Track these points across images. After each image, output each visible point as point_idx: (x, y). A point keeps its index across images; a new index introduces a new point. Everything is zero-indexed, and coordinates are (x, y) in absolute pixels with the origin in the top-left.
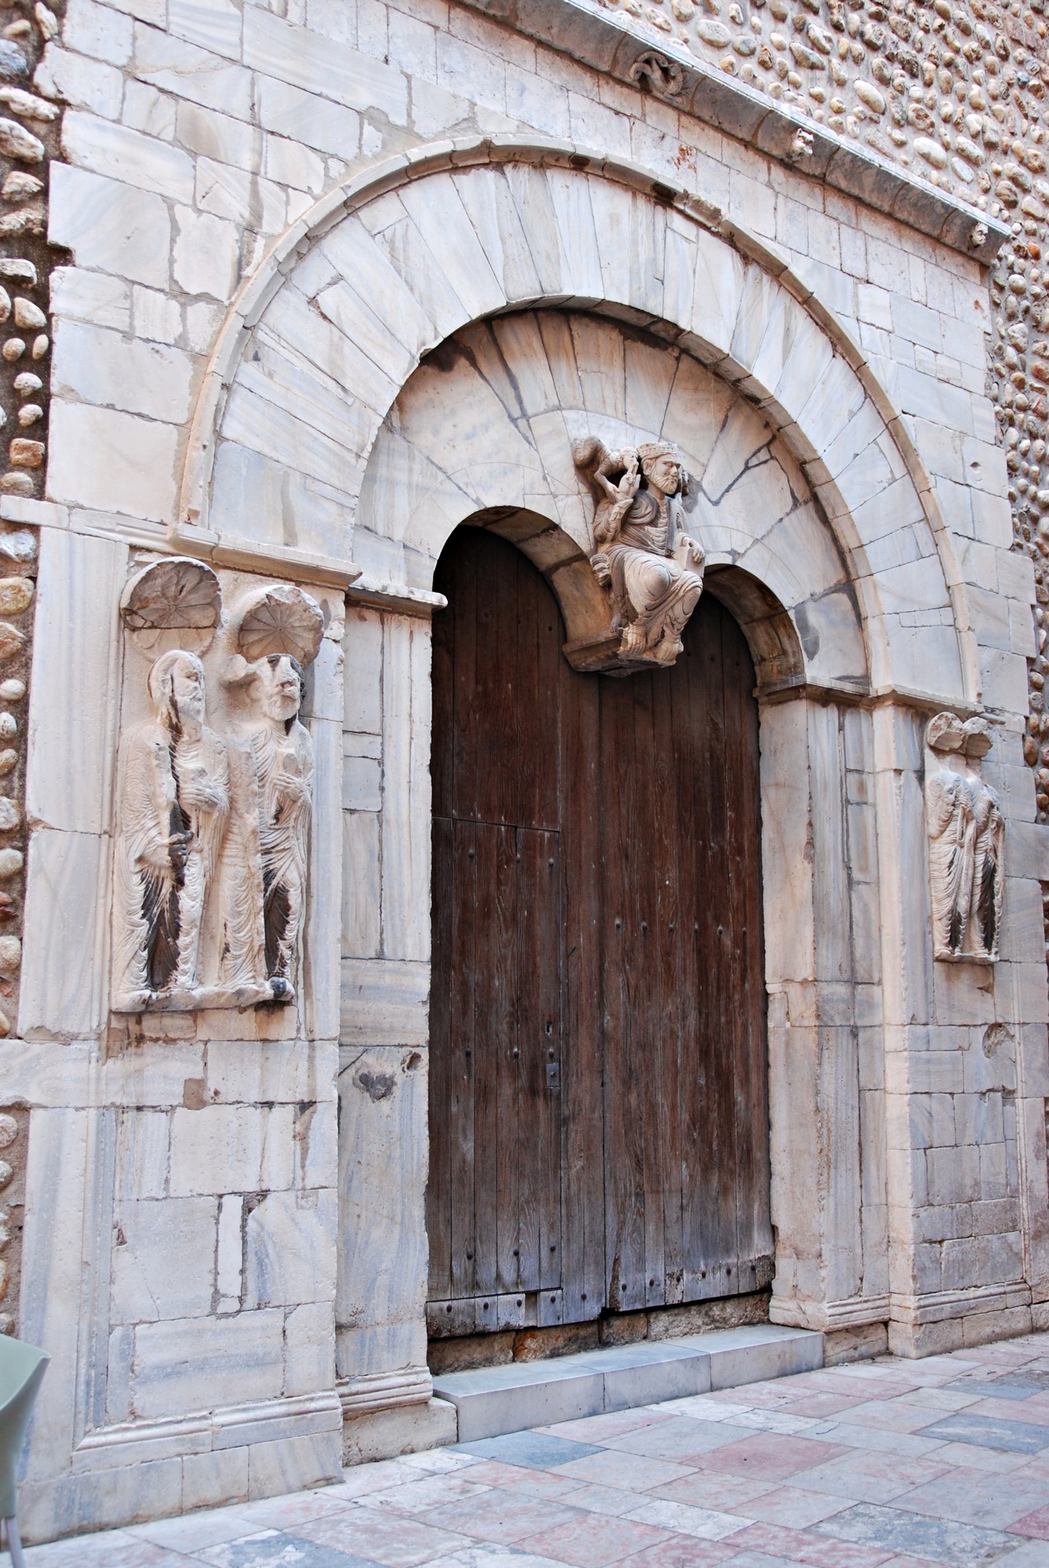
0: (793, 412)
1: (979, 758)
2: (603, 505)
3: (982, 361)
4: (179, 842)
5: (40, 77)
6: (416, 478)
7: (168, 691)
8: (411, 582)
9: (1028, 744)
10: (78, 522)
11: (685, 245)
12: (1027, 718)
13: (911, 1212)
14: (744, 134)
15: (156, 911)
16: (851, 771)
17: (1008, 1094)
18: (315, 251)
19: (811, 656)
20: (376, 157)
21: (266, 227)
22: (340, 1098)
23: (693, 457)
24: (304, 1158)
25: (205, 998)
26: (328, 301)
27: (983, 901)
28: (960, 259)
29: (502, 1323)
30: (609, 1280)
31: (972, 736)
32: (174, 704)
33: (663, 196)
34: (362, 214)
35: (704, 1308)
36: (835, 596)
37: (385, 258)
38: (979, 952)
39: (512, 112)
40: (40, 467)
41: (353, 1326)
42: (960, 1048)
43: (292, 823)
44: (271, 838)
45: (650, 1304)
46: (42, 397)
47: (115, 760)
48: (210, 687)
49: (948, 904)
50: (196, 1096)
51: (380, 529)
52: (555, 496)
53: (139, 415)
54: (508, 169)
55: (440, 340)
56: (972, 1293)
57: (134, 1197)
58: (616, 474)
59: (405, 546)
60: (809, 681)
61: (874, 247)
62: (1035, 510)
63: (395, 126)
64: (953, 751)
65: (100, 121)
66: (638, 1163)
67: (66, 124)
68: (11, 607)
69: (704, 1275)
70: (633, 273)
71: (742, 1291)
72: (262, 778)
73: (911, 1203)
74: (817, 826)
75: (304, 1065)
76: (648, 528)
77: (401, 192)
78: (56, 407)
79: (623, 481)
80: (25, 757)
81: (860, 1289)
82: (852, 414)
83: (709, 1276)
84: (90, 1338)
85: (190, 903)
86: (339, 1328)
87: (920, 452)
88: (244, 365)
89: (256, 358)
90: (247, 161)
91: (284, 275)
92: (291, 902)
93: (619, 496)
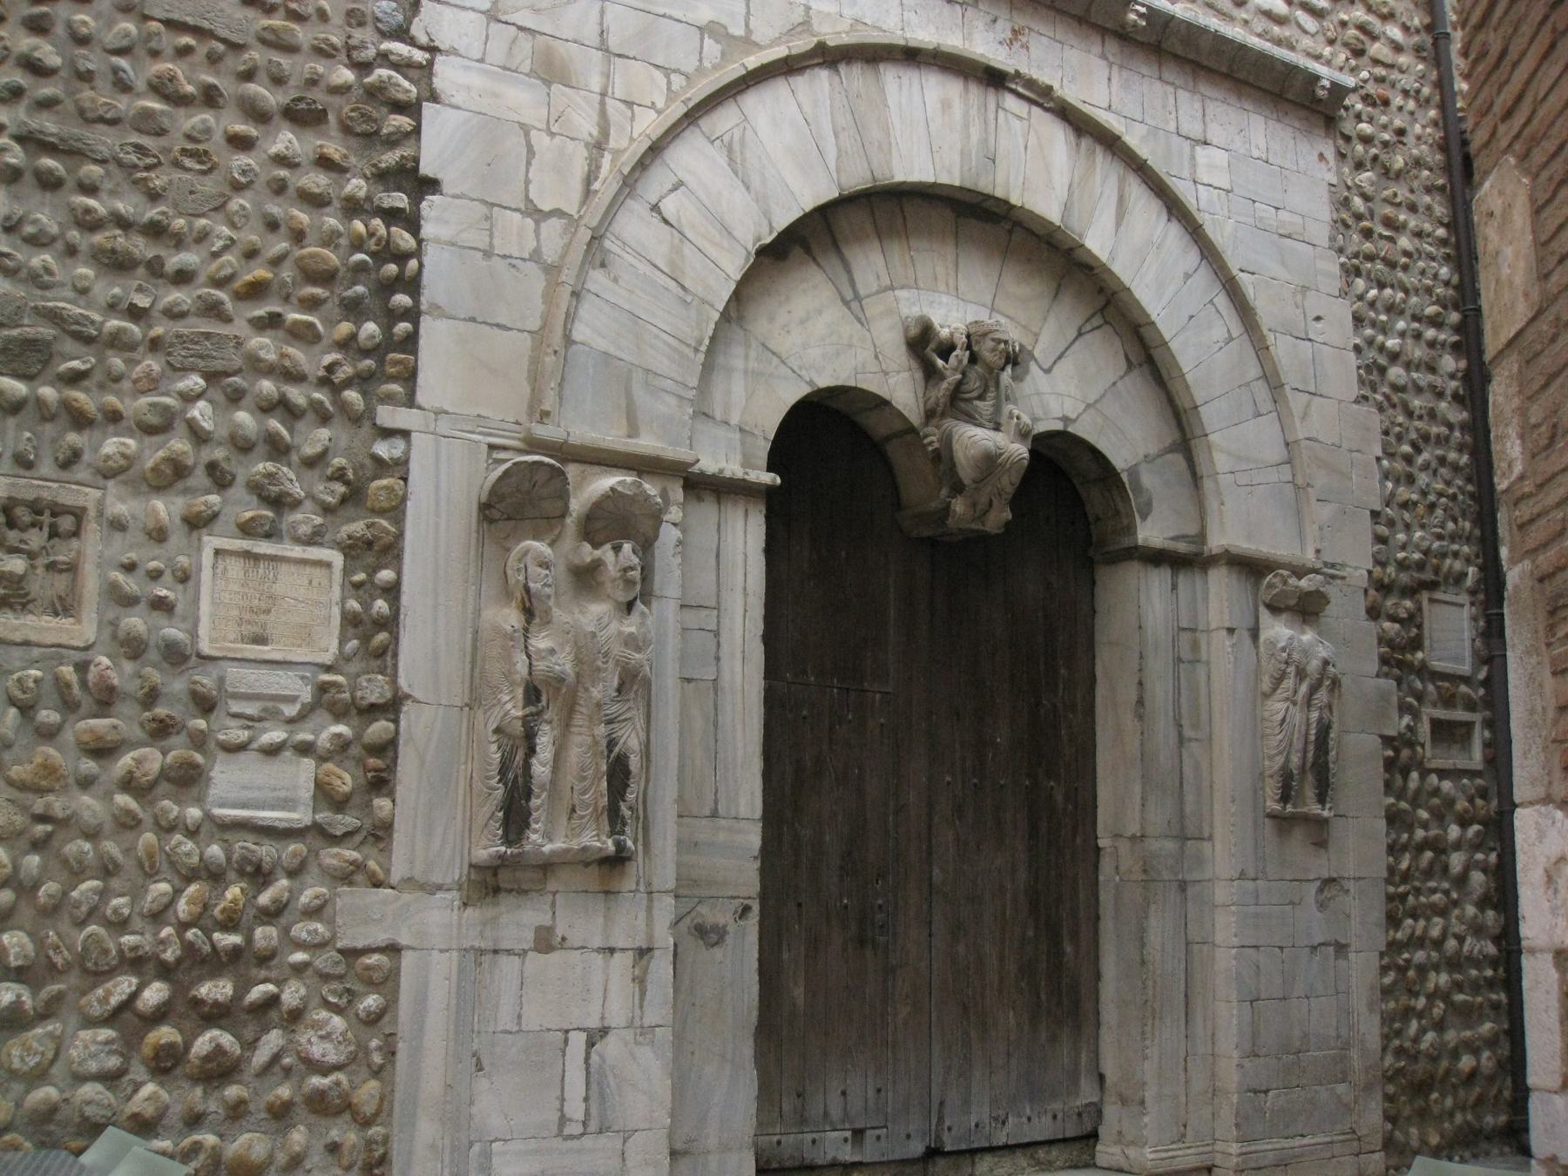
0: (1126, 279)
1: (1317, 614)
2: (932, 382)
3: (1324, 212)
4: (532, 714)
5: (417, 30)
6: (752, 365)
7: (521, 578)
8: (746, 464)
9: (1370, 599)
10: (444, 426)
11: (1016, 124)
12: (1370, 572)
13: (1235, 1062)
14: (1077, 11)
15: (511, 776)
16: (1184, 629)
17: (1341, 949)
18: (658, 162)
19: (1144, 517)
20: (715, 68)
21: (612, 144)
22: (675, 945)
23: (1024, 327)
24: (642, 999)
25: (553, 852)
26: (669, 206)
27: (1317, 757)
28: (1303, 113)
29: (829, 1157)
30: (934, 1121)
31: (1309, 594)
32: (527, 589)
33: (994, 79)
34: (702, 122)
35: (1029, 1151)
36: (1169, 456)
37: (722, 160)
38: (1315, 809)
39: (845, 12)
40: (410, 377)
41: (686, 1153)
42: (1292, 903)
43: (632, 695)
44: (613, 709)
45: (975, 1146)
46: (413, 314)
47: (475, 640)
48: (560, 570)
49: (1280, 760)
50: (545, 941)
51: (718, 415)
52: (886, 373)
53: (498, 325)
54: (842, 68)
55: (775, 234)
56: (1298, 1142)
57: (491, 1030)
58: (946, 350)
59: (741, 430)
60: (1140, 542)
61: (1212, 108)
62: (1382, 361)
63: (733, 37)
64: (1288, 609)
65: (467, 62)
66: (965, 1008)
67: (437, 67)
68: (385, 505)
69: (1029, 1119)
70: (964, 154)
71: (1068, 1135)
72: (606, 655)
73: (1235, 1054)
74: (1148, 686)
75: (642, 915)
76: (977, 403)
77: (739, 98)
78: (426, 323)
79: (952, 359)
80: (397, 639)
81: (1184, 1136)
82: (1187, 276)
83: (1035, 1120)
84: (452, 1152)
85: (541, 769)
86: (673, 1154)
87: (1258, 311)
88: (591, 272)
89: (603, 265)
90: (596, 84)
91: (628, 185)
92: (632, 768)
93: (948, 373)
